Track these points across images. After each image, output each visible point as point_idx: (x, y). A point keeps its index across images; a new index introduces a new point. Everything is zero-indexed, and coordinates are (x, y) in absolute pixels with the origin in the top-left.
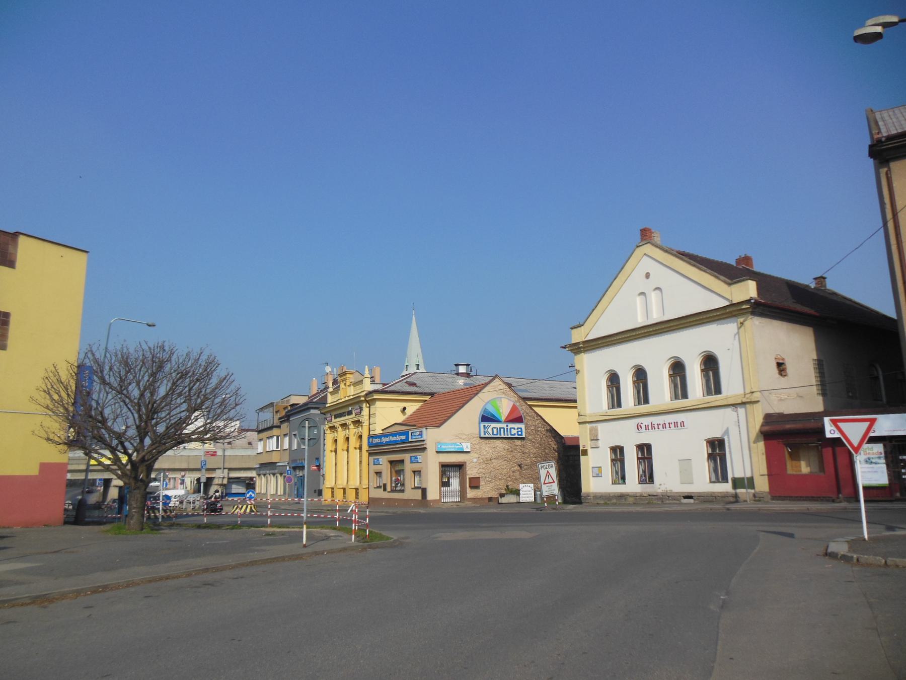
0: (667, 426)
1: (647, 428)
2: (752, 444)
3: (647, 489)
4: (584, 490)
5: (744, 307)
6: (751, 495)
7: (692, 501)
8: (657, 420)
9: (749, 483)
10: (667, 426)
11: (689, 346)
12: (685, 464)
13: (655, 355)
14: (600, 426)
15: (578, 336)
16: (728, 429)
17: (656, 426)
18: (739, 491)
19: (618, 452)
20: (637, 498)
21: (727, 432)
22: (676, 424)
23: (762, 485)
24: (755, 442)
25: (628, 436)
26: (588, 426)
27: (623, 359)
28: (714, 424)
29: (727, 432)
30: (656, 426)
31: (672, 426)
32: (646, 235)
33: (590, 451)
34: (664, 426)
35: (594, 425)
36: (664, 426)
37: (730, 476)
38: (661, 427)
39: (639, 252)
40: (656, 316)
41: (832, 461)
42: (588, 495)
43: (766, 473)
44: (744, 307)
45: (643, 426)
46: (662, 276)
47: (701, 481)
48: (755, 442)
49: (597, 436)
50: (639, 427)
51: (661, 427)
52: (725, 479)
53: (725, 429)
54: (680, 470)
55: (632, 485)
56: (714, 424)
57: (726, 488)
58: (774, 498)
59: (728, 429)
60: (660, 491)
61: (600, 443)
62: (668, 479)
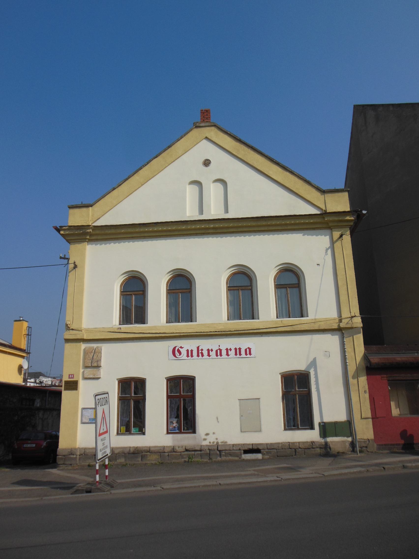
0: (224, 352)
1: (190, 354)
2: (351, 380)
3: (185, 440)
4: (64, 443)
5: (348, 218)
6: (348, 445)
7: (259, 456)
8: (205, 344)
9: (346, 428)
10: (224, 352)
11: (264, 255)
12: (250, 411)
13: (210, 263)
14: (105, 348)
15: (77, 218)
16: (315, 359)
17: (205, 353)
18: (329, 439)
19: (133, 391)
20: (165, 458)
21: (314, 363)
22: (238, 351)
23: (365, 430)
24: (356, 376)
25: (155, 365)
26: (83, 346)
27: (156, 261)
28: (294, 353)
29: (314, 363)
30: (205, 353)
31: (232, 353)
32: (205, 118)
33: (82, 384)
34: (219, 353)
35: (94, 345)
36: (219, 353)
37: (317, 420)
38: (213, 354)
39: (195, 133)
40: (214, 211)
41: (308, 197)
42: (72, 452)
43: (370, 415)
44: (348, 218)
45: (184, 352)
46: (226, 165)
47: (273, 429)
48: (356, 376)
49: (99, 360)
50: (175, 352)
51: (213, 354)
52: (308, 424)
53: (311, 359)
54: (240, 403)
55: (157, 432)
56: (294, 353)
57: (312, 436)
58: (381, 447)
59: (315, 359)
60: (205, 443)
61: (102, 372)
62: (218, 423)
